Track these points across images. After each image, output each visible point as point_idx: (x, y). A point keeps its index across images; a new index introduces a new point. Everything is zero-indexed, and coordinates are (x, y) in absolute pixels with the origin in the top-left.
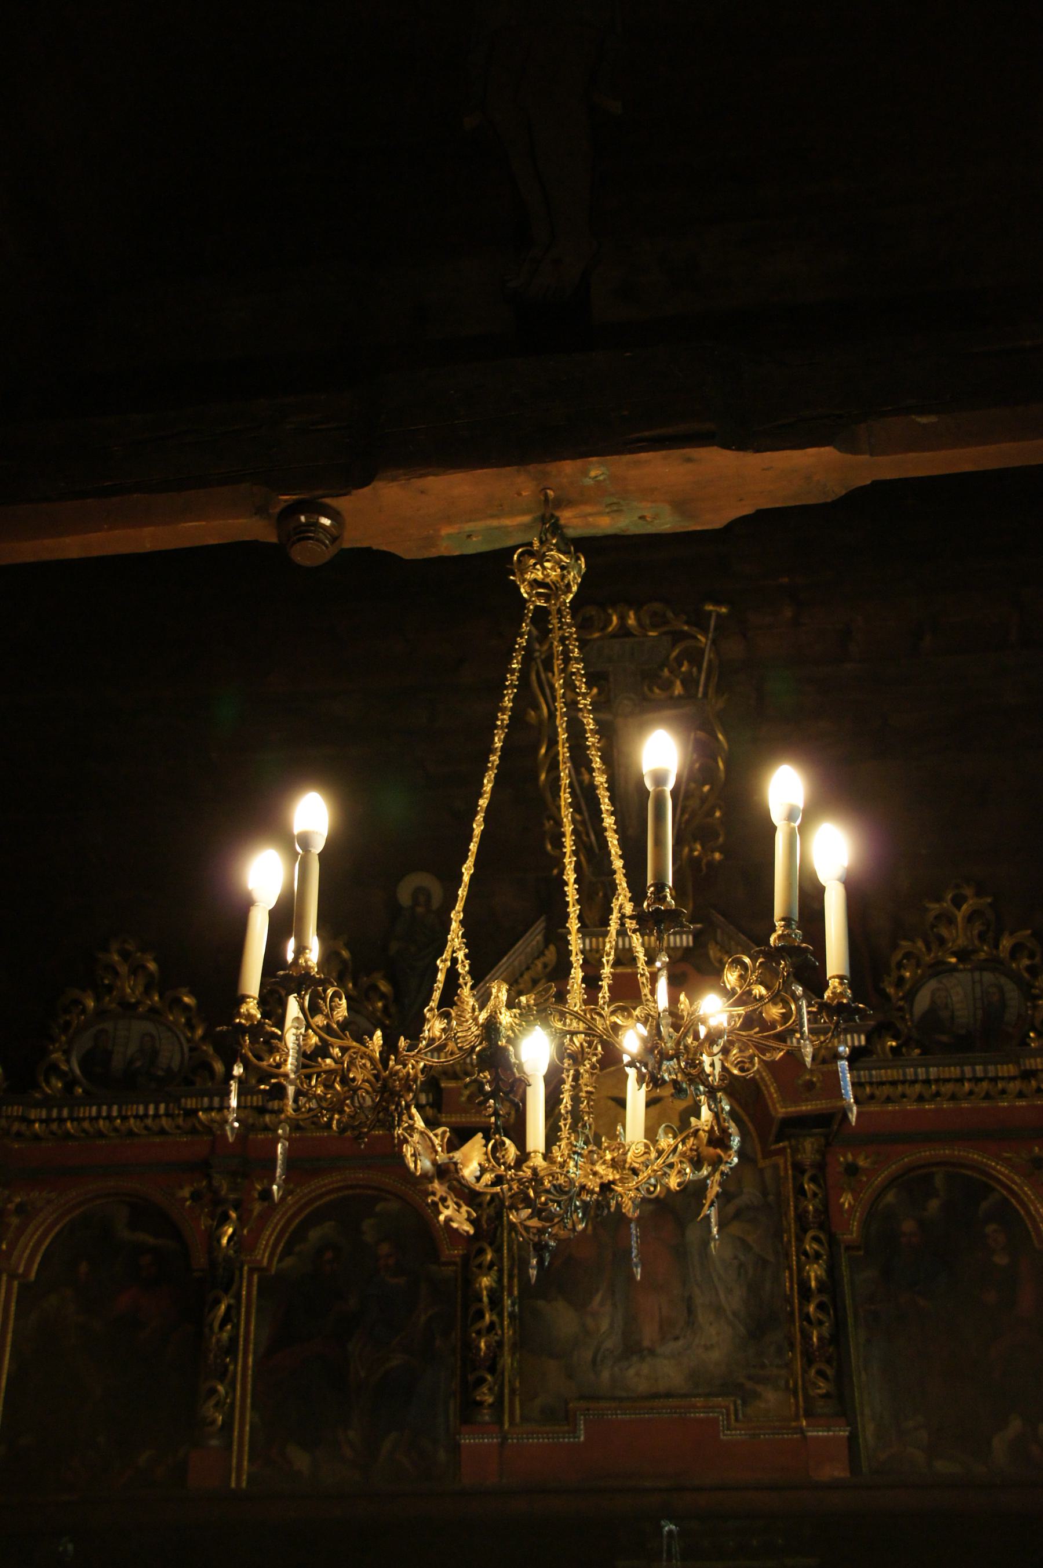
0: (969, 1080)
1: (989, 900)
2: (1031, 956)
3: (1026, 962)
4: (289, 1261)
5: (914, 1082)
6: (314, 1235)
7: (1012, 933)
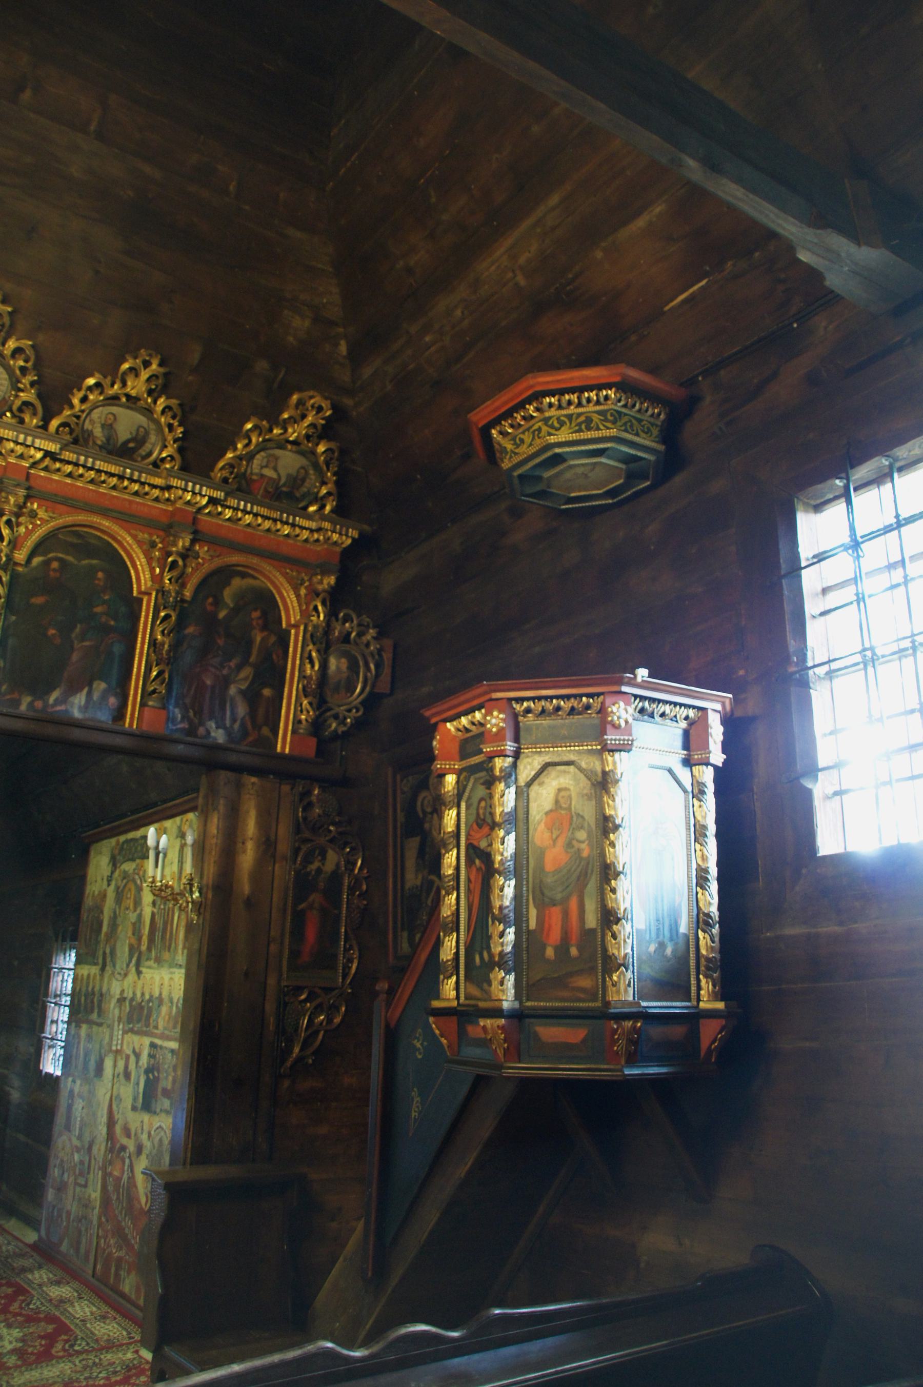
0: (128, 479)
1: (10, 309)
2: (26, 361)
3: (21, 363)
5: (91, 469)
7: (17, 340)
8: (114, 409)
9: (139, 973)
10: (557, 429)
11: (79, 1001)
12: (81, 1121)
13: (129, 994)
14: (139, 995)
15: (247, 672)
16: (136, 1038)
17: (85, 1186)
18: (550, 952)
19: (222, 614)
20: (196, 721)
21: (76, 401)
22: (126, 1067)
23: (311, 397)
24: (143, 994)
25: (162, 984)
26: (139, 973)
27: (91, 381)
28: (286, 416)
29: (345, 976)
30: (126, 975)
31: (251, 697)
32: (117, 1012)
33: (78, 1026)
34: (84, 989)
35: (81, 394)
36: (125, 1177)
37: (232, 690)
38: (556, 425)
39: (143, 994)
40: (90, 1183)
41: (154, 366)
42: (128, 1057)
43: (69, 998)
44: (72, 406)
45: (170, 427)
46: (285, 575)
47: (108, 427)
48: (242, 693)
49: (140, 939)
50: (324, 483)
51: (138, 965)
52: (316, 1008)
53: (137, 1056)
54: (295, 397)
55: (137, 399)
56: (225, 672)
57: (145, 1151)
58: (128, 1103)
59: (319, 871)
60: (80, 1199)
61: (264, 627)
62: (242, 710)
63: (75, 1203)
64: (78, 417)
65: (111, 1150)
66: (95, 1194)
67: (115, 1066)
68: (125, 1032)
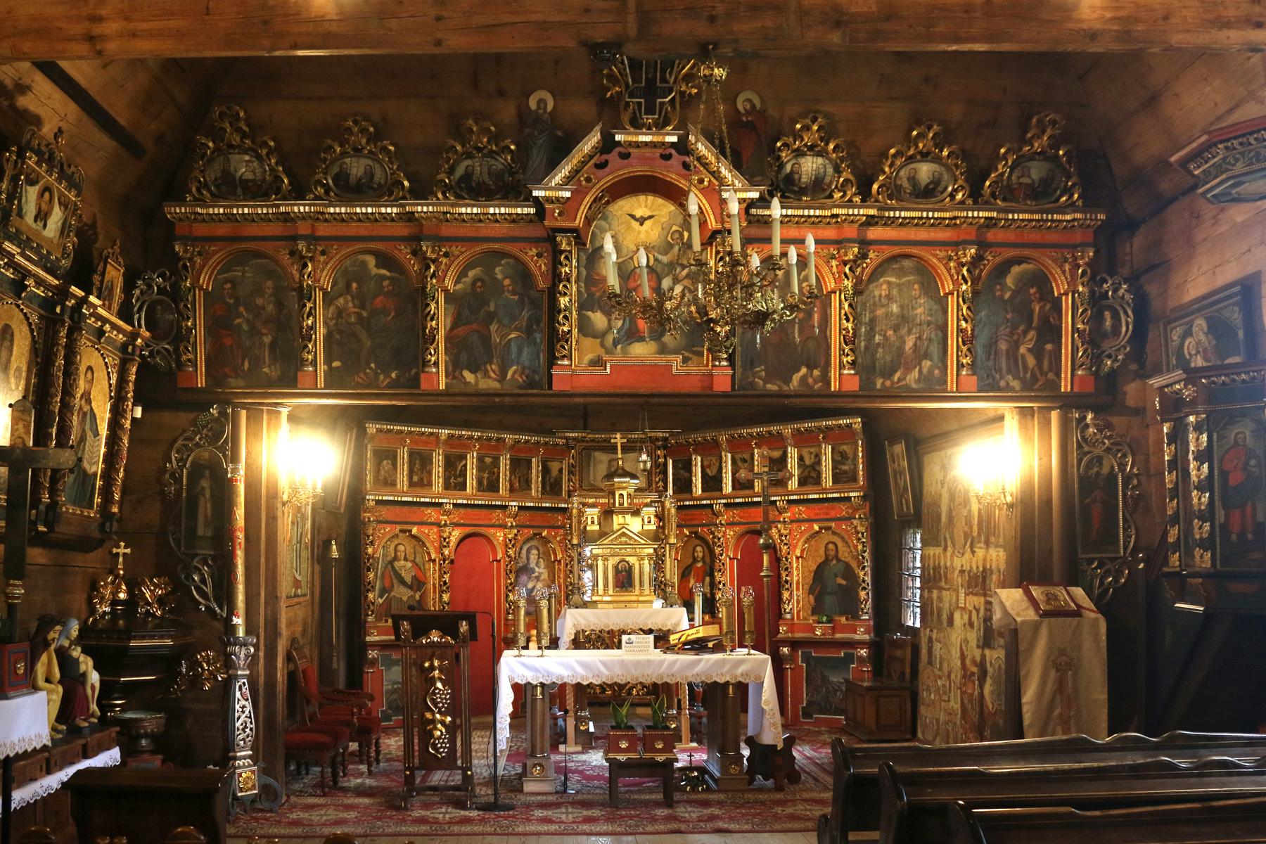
4: (459, 286)
6: (471, 274)
8: (913, 166)
9: (973, 552)
10: (1233, 165)
11: (929, 574)
12: (941, 657)
13: (967, 568)
14: (974, 568)
15: (1032, 334)
16: (975, 598)
17: (949, 701)
18: (1234, 537)
19: (1007, 296)
20: (998, 376)
21: (887, 169)
22: (970, 618)
23: (1047, 116)
24: (978, 567)
25: (134, 35)
26: (973, 552)
27: (892, 151)
28: (1029, 135)
29: (1125, 548)
30: (963, 554)
31: (1037, 352)
32: (960, 579)
33: (930, 592)
34: (931, 565)
35: (889, 161)
36: (976, 692)
37: (1022, 350)
38: (1232, 161)
39: (978, 567)
40: (952, 698)
41: (935, 127)
42: (971, 612)
43: (919, 571)
44: (884, 172)
45: (957, 166)
46: (1049, 257)
47: (913, 179)
48: (1029, 350)
49: (971, 528)
50: (1068, 178)
51: (972, 546)
52: (1105, 572)
53: (978, 611)
54: (1034, 120)
55: (928, 154)
56: (1015, 337)
57: (989, 675)
58: (973, 643)
59: (1098, 473)
60: (945, 710)
61: (1041, 299)
62: (1031, 361)
63: (942, 713)
64: (890, 178)
65: (964, 676)
66: (957, 706)
67: (962, 618)
68: (966, 595)
